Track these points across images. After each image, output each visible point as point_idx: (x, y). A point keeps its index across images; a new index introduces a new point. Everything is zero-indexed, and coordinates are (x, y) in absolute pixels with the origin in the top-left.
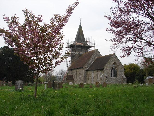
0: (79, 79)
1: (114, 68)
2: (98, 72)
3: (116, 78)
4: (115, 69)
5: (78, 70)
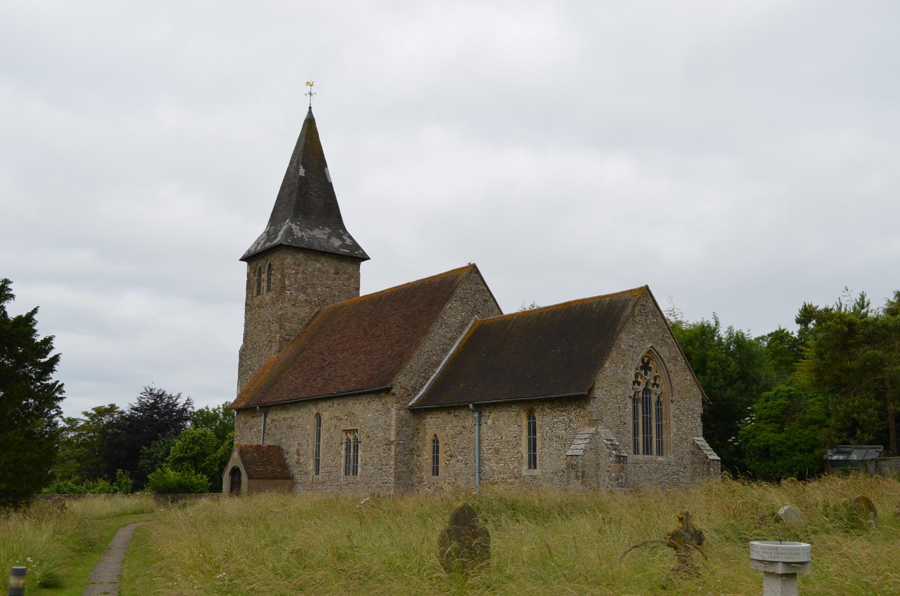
0: (351, 468)
1: (646, 390)
2: (531, 417)
3: (660, 459)
4: (654, 398)
5: (329, 411)
